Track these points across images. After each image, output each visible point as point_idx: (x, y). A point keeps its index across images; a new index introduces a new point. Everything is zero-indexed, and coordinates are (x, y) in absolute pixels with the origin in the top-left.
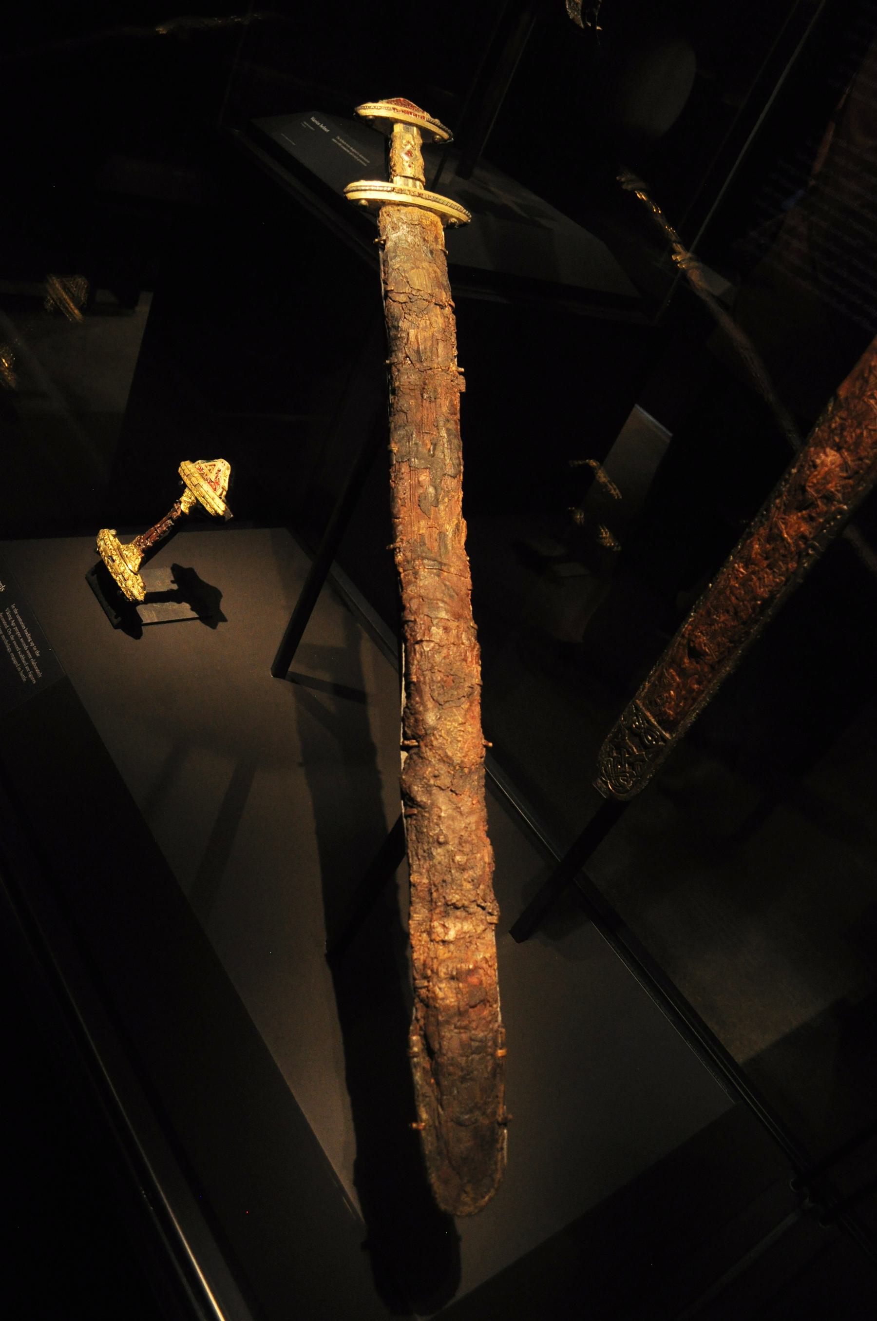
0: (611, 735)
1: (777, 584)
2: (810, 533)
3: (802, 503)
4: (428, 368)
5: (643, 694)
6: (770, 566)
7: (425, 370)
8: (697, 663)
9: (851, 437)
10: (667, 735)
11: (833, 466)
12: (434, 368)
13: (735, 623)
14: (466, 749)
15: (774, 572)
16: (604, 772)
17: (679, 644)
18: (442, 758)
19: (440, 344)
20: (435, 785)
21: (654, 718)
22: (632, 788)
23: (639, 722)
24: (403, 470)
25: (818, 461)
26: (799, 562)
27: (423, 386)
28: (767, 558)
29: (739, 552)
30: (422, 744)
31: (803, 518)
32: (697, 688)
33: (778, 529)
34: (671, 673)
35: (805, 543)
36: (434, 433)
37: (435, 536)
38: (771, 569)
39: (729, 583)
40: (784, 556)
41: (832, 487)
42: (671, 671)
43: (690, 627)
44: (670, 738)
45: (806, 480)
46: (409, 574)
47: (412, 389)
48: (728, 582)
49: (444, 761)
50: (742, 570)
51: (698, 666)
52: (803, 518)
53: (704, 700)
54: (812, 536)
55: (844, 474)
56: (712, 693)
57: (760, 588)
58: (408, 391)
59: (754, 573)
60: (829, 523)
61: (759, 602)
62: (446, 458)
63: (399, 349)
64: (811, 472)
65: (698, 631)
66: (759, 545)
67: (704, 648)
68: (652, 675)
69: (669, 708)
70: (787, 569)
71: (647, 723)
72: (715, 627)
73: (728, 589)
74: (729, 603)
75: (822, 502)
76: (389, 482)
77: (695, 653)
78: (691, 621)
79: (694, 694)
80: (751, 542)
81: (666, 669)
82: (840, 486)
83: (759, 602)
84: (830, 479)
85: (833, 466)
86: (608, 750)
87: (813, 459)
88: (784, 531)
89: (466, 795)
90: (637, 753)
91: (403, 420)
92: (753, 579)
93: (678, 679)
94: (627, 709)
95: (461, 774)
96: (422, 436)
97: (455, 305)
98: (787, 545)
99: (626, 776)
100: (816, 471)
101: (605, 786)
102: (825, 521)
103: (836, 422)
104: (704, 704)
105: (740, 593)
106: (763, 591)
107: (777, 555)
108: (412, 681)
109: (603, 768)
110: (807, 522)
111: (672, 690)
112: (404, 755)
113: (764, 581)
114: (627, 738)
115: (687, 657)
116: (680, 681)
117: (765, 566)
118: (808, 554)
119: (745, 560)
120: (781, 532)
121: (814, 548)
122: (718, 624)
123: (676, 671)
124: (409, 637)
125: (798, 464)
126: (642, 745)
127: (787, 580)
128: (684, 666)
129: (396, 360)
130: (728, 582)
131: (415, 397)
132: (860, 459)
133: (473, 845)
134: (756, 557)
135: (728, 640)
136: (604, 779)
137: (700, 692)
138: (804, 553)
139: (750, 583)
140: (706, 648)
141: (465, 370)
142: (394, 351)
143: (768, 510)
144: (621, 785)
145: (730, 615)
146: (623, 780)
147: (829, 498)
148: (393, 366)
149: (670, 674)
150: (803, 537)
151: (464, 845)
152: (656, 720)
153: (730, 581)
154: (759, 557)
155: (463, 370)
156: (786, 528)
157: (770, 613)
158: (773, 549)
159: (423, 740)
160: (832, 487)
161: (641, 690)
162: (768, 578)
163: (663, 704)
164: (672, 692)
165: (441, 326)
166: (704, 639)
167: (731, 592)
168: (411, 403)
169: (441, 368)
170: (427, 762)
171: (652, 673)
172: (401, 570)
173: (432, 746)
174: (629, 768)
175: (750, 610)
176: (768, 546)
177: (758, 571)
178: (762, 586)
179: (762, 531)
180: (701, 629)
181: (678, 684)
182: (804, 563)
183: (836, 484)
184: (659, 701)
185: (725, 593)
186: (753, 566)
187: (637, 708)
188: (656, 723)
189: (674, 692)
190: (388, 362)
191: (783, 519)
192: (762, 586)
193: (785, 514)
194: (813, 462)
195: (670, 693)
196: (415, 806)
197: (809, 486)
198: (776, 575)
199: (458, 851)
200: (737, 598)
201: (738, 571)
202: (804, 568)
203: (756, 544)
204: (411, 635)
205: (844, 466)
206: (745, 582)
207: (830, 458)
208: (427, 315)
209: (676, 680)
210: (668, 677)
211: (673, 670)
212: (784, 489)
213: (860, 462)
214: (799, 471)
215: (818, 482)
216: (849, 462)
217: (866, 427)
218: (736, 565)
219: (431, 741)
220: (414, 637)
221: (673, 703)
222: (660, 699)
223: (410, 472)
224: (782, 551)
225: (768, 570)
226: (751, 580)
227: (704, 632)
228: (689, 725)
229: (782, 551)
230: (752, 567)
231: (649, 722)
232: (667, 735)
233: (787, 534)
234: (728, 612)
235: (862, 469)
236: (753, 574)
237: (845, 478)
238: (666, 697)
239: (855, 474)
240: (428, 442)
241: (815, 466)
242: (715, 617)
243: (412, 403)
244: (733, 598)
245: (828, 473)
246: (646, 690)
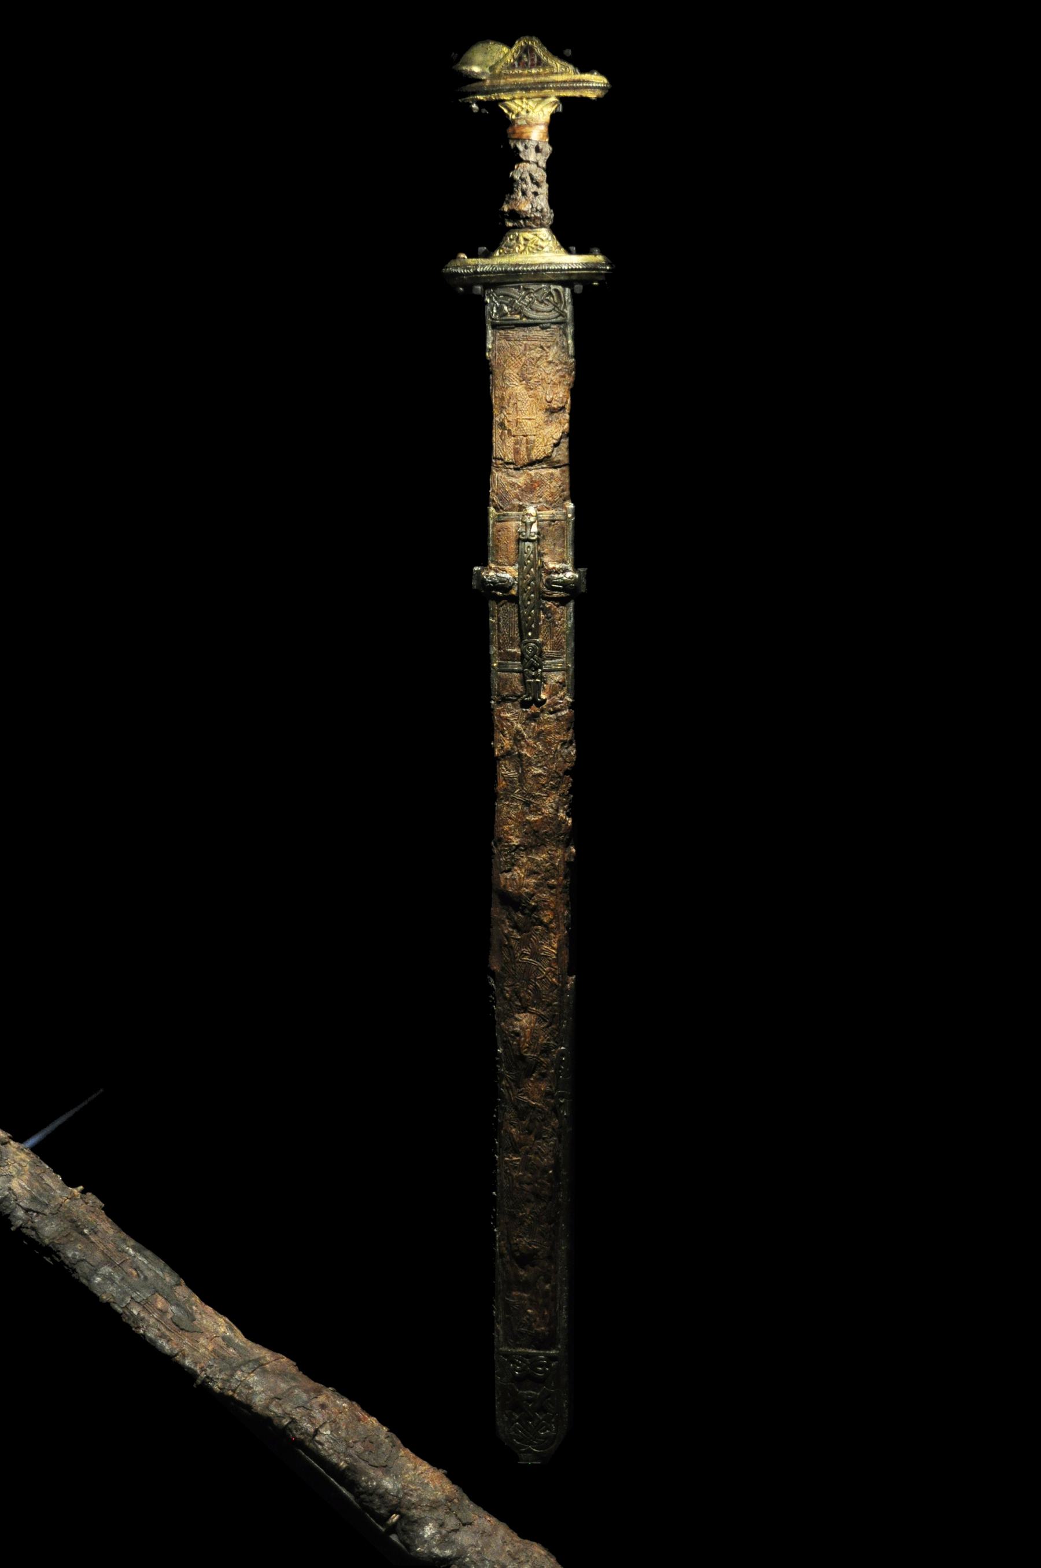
0: (498, 1403)
1: (554, 1146)
2: (551, 1087)
3: (524, 1067)
4: (59, 1206)
5: (501, 1339)
6: (538, 1137)
7: (58, 1210)
8: (533, 1266)
9: (529, 994)
10: (553, 1352)
11: (532, 1025)
12: (62, 1203)
13: (543, 1205)
14: (438, 1485)
15: (544, 1139)
16: (518, 1443)
17: (503, 1265)
18: (431, 1506)
19: (44, 1177)
20: (449, 1532)
21: (529, 1348)
22: (557, 1430)
23: (519, 1365)
24: (135, 1312)
25: (518, 1029)
26: (558, 1115)
27: (74, 1225)
28: (530, 1133)
29: (500, 1147)
30: (404, 1511)
31: (537, 1080)
32: (550, 1286)
33: (524, 1103)
34: (515, 1295)
35: (552, 1098)
36: (128, 1258)
37: (222, 1343)
38: (539, 1139)
39: (512, 1177)
40: (543, 1120)
41: (543, 1040)
42: (514, 1293)
43: (502, 1242)
44: (558, 1352)
45: (519, 1049)
46: (241, 1390)
47: (67, 1235)
48: (510, 1177)
49: (435, 1508)
50: (515, 1158)
51: (536, 1268)
52: (537, 1080)
53: (563, 1294)
54: (554, 1088)
55: (545, 1024)
56: (565, 1280)
57: (542, 1160)
58: (65, 1239)
59: (527, 1153)
60: (560, 1069)
61: (551, 1172)
62: (158, 1272)
63: (13, 1210)
64: (518, 1041)
65: (514, 1238)
66: (515, 1127)
67: (530, 1248)
68: (497, 1315)
69: (539, 1326)
70: (553, 1129)
71: (527, 1358)
72: (527, 1223)
73: (515, 1181)
74: (525, 1192)
75: (543, 1057)
76: (134, 1331)
77: (525, 1259)
78: (499, 1238)
79: (551, 1294)
80: (506, 1131)
81: (508, 1297)
82: (548, 1036)
83: (551, 1172)
84: (537, 1035)
85: (532, 1025)
86: (506, 1419)
87: (510, 1030)
88: (530, 1101)
89: (476, 1519)
90: (538, 1394)
91: (87, 1266)
92: (531, 1158)
93: (526, 1295)
94: (497, 1366)
95: (456, 1507)
96: (120, 1268)
97: (11, 1134)
98: (540, 1109)
99: (544, 1425)
100: (521, 1037)
101: (529, 1455)
102: (556, 1070)
103: (507, 992)
104: (565, 1296)
105: (529, 1178)
106: (548, 1161)
107: (537, 1124)
108: (342, 1469)
109: (515, 1440)
110: (542, 1080)
111: (528, 1309)
112: (394, 1538)
113: (542, 1152)
114: (517, 1390)
115: (521, 1269)
116: (529, 1295)
117: (533, 1140)
118: (561, 1104)
119: (511, 1149)
120: (528, 1103)
121: (562, 1096)
122: (528, 1218)
123: (519, 1290)
124: (302, 1437)
125: (499, 1043)
126: (538, 1382)
127: (559, 1136)
128: (523, 1278)
129: (21, 1222)
130: (510, 1177)
131: (76, 1240)
132: (549, 1005)
133: (523, 1550)
134: (520, 1138)
135: (547, 1224)
136: (524, 1449)
137: (554, 1288)
138: (558, 1106)
139: (530, 1163)
140: (533, 1246)
141: (83, 1186)
142: (8, 1215)
143: (502, 1096)
144: (545, 1438)
145: (533, 1202)
146: (544, 1431)
147: (546, 1050)
148: (21, 1229)
149: (515, 1298)
150: (548, 1094)
151: (517, 1557)
152: (533, 1349)
153: (510, 1174)
154: (522, 1137)
155: (81, 1188)
156: (529, 1098)
157: (565, 1173)
158: (531, 1121)
159: (401, 1507)
160: (543, 1040)
161: (497, 1336)
162: (544, 1147)
163: (530, 1328)
164: (529, 1311)
165: (29, 1161)
166: (525, 1240)
167: (521, 1183)
168: (79, 1248)
169: (68, 1198)
170: (424, 1520)
171: (494, 1313)
172: (230, 1393)
173: (413, 1504)
174: (540, 1415)
175: (548, 1184)
176: (524, 1122)
177: (531, 1148)
178: (543, 1158)
179: (508, 1116)
180: (516, 1234)
181: (530, 1299)
182: (563, 1113)
183: (544, 1036)
184: (522, 1329)
185: (516, 1187)
186: (523, 1148)
187: (506, 1355)
188: (535, 1351)
189: (531, 1309)
190: (13, 1229)
191: (521, 1092)
192: (543, 1158)
193: (519, 1088)
194: (513, 1032)
195: (528, 1314)
196: (451, 1562)
197: (526, 1052)
198: (548, 1140)
199: (519, 1565)
200: (528, 1184)
201: (512, 1162)
202: (566, 1117)
203: (511, 1129)
204: (302, 1434)
205: (541, 1018)
206: (526, 1165)
207: (524, 1021)
208: (9, 1160)
209: (524, 1296)
210: (515, 1301)
211: (515, 1291)
212: (502, 1070)
213: (551, 1007)
214: (504, 1048)
215: (530, 1045)
216: (543, 1013)
217: (535, 979)
218: (507, 1159)
219: (410, 1501)
220: (306, 1433)
221: (538, 1319)
222: (522, 1327)
223: (144, 1307)
224: (540, 1117)
225: (538, 1141)
226: (530, 1160)
227: (521, 1234)
228: (566, 1325)
229: (540, 1117)
230: (522, 1150)
231: (528, 1356)
232: (553, 1352)
233: (534, 1102)
234: (529, 1201)
235: (555, 1011)
236: (528, 1154)
237: (548, 1027)
238: (528, 1319)
239: (553, 1019)
240: (130, 1270)
241: (518, 1034)
242: (521, 1214)
243: (80, 1247)
244: (525, 1186)
245: (531, 1033)
246: (501, 1333)
